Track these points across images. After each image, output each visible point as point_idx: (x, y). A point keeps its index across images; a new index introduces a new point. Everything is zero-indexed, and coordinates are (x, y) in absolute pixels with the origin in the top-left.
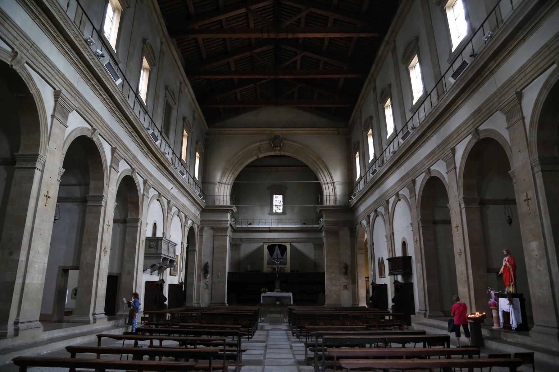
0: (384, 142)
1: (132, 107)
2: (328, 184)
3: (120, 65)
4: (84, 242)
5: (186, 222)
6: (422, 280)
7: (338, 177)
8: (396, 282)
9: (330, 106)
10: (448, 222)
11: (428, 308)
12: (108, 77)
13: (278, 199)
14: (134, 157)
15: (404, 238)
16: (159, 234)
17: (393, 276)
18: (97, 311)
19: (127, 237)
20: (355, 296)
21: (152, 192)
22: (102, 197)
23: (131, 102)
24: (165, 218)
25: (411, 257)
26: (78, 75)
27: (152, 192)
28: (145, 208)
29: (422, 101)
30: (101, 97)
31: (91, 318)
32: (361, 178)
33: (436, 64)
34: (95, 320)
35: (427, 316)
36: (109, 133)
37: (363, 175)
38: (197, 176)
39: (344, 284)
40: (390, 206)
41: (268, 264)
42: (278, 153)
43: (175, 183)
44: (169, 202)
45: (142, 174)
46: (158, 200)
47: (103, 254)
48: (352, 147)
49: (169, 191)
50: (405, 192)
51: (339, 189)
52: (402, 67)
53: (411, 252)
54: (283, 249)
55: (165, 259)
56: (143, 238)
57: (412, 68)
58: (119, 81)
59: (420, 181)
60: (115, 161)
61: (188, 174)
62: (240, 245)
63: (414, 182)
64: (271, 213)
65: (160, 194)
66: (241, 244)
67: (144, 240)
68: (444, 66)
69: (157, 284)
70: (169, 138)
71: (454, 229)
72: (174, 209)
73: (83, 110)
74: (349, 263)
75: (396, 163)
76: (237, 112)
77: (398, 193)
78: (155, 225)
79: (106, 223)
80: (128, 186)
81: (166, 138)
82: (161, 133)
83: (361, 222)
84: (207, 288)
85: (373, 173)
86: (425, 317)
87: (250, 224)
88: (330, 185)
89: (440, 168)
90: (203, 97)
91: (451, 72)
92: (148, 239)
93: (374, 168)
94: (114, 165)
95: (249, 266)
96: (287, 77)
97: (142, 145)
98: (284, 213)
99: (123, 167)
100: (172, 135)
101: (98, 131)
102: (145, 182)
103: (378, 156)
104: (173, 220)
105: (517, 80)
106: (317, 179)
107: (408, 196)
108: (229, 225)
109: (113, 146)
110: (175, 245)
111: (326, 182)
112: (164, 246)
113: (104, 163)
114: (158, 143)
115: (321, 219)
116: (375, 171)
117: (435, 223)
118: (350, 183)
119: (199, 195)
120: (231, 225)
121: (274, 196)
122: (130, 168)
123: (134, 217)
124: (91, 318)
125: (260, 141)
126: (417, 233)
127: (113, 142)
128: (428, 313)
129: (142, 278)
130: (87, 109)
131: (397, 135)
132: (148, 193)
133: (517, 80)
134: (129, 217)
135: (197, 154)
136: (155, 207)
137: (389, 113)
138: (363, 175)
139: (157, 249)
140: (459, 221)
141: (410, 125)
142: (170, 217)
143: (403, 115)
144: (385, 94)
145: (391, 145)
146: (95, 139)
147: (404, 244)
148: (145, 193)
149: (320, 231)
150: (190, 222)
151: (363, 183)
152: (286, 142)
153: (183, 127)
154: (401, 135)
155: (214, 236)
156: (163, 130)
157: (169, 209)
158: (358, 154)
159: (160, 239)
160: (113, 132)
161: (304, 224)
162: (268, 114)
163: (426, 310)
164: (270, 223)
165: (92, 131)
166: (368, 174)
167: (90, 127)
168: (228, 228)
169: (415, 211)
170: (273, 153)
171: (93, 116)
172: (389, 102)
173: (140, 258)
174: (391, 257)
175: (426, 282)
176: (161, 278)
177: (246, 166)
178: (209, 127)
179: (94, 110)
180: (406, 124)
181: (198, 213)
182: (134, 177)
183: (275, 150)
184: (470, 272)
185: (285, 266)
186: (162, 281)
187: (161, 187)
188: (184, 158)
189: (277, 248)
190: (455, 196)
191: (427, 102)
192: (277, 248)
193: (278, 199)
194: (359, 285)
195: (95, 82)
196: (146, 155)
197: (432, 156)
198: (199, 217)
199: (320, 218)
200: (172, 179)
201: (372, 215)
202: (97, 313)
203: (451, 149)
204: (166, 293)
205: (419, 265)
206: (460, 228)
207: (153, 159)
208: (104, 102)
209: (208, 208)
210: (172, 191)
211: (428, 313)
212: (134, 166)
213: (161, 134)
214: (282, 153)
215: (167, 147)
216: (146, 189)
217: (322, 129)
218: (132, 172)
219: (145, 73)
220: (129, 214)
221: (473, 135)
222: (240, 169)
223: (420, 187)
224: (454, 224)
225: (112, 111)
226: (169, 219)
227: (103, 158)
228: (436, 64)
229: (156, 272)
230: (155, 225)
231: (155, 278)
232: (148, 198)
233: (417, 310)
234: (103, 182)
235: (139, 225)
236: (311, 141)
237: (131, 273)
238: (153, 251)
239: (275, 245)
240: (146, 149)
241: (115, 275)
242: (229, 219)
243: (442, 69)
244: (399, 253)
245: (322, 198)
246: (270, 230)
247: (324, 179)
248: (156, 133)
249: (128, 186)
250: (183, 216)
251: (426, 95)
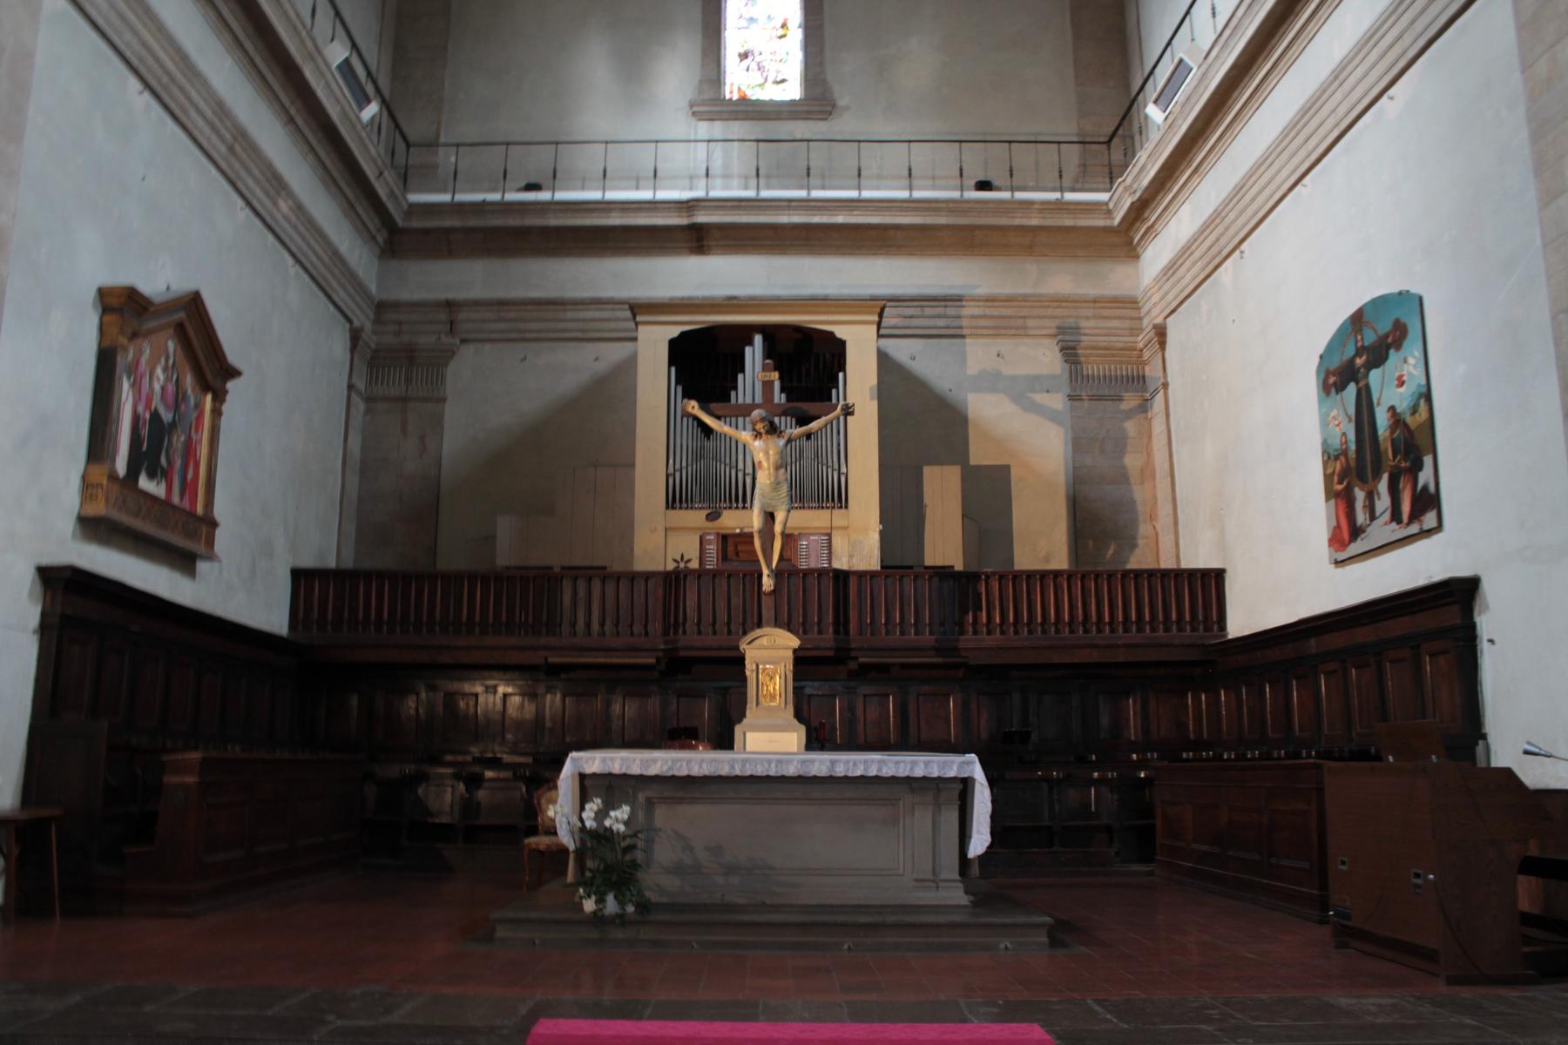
41: (674, 501)
54: (809, 364)
62: (440, 359)
66: (452, 353)
87: (532, 187)
95: (505, 528)
98: (819, 97)
105: (1232, 216)
109: (356, 323)
133: (1232, 216)
155: (1347, 934)
164: (686, 165)
185: (839, 517)
189: (754, 354)
192: (754, 354)
203: (1155, 327)
225: (350, 208)
239: (743, 334)
246: (697, 236)
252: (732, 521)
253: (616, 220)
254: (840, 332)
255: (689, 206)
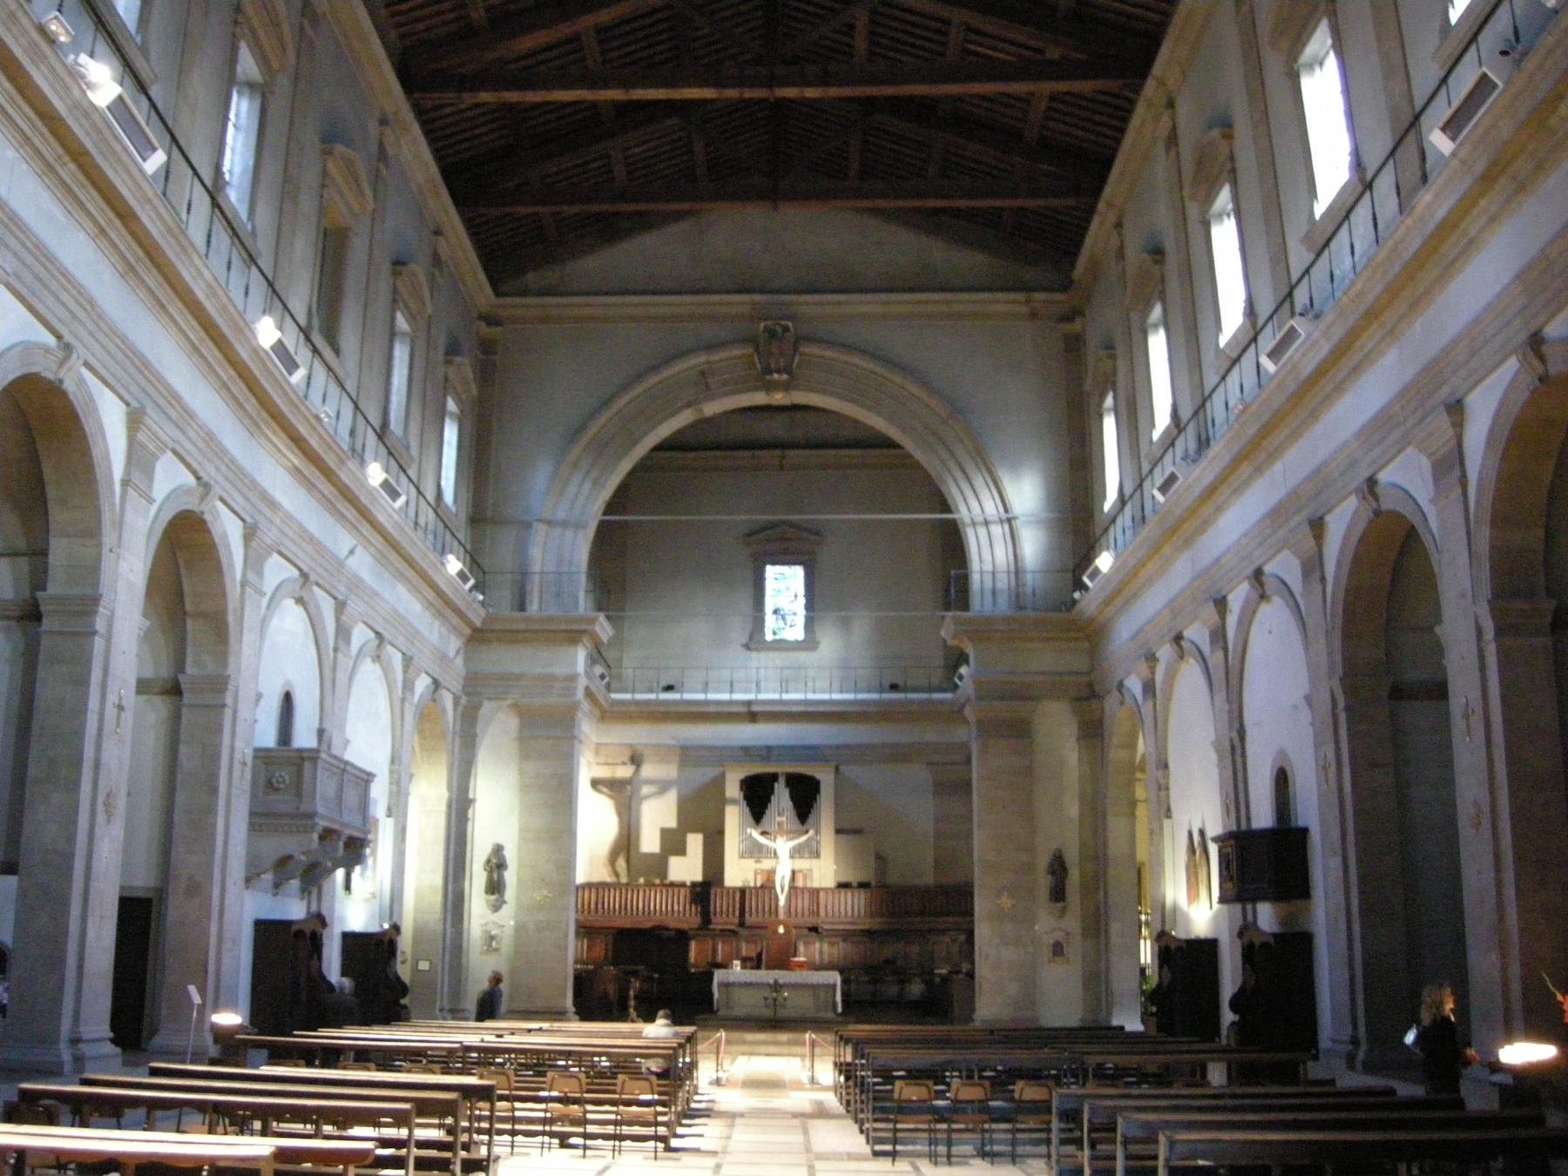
0: (1208, 357)
1: (203, 250)
2: (986, 523)
3: (155, 91)
4: (32, 772)
5: (408, 686)
6: (1343, 926)
7: (1026, 492)
8: (1245, 930)
9: (998, 203)
10: (1439, 691)
11: (1362, 1030)
12: (118, 148)
13: (785, 585)
14: (210, 437)
15: (1282, 754)
16: (304, 738)
17: (1238, 907)
18: (87, 1031)
19: (184, 750)
20: (1097, 983)
21: (277, 571)
22: (95, 600)
23: (197, 228)
24: (327, 672)
25: (1304, 832)
26: (11, 153)
27: (277, 571)
28: (249, 638)
29: (1343, 212)
30: (89, 225)
31: (66, 1056)
32: (1122, 500)
33: (1398, 69)
34: (79, 1060)
35: (1359, 1067)
36: (119, 356)
37: (1128, 491)
38: (449, 497)
39: (1049, 940)
40: (1232, 621)
42: (779, 398)
43: (365, 528)
44: (340, 606)
45: (239, 502)
46: (300, 601)
47: (101, 817)
48: (1077, 387)
49: (340, 564)
50: (1285, 566)
51: (1033, 545)
52: (1273, 65)
53: (1310, 811)
55: (327, 834)
56: (244, 751)
57: (1310, 67)
58: (156, 161)
59: (1343, 520)
60: (140, 460)
61: (413, 490)
63: (1317, 527)
64: (755, 639)
65: (304, 575)
67: (249, 760)
68: (1425, 75)
69: (299, 934)
70: (337, 351)
71: (1458, 724)
72: (360, 635)
73: (29, 278)
74: (1072, 856)
75: (1256, 451)
76: (610, 230)
77: (1372, 482)
78: (288, 699)
79: (112, 699)
80: (185, 544)
81: (327, 352)
82: (306, 332)
83: (1120, 686)
84: (673, 1077)
85: (1164, 489)
86: (1351, 1066)
87: (669, 688)
88: (997, 530)
89: (1408, 476)
90: (467, 177)
91: (1442, 111)
92: (262, 755)
93: (1167, 467)
94: (136, 476)
96: (811, 93)
97: (239, 388)
98: (810, 643)
99: (169, 478)
100: (349, 337)
101: (82, 350)
102: (250, 534)
103: (1185, 414)
104: (359, 677)
106: (945, 506)
107: (1294, 579)
108: (580, 694)
109: (135, 404)
110: (366, 779)
111: (980, 519)
112: (325, 786)
113: (100, 473)
114: (298, 377)
115: (963, 670)
116: (1172, 478)
117: (1398, 693)
118: (1077, 523)
119: (461, 575)
120: (589, 693)
121: (769, 568)
122: (192, 480)
123: (211, 668)
124: (66, 1056)
125: (709, 347)
126: (1329, 734)
127: (133, 388)
128: (1361, 1056)
129: (242, 907)
130: (43, 273)
131: (1255, 339)
132: (260, 574)
134: (190, 670)
135: (451, 405)
136: (289, 622)
137: (1225, 238)
138: (1128, 491)
139: (299, 795)
140: (1475, 695)
141: (1301, 297)
142: (345, 663)
143: (1280, 256)
144: (1211, 170)
145: (1233, 379)
146: (69, 385)
147: (1282, 779)
148: (251, 576)
149: (955, 714)
150: (422, 684)
151: (1128, 522)
152: (815, 350)
153: (394, 301)
154: (1268, 341)
156: (316, 322)
157: (343, 632)
158: (1109, 401)
159: (311, 756)
160: (135, 352)
161: (894, 687)
162: (738, 232)
163: (1355, 1042)
165: (60, 354)
166: (1147, 485)
167: (51, 340)
168: (575, 707)
169: (1320, 645)
170: (760, 398)
171: (65, 297)
172: (1224, 198)
173: (233, 830)
174: (1234, 828)
175: (1357, 928)
176: (314, 908)
177: (658, 448)
178: (498, 294)
179: (65, 274)
180: (1290, 295)
181: (454, 645)
182: (207, 517)
183: (769, 387)
184: (1510, 891)
186: (320, 920)
187: (310, 549)
188: (395, 424)
190: (1463, 596)
191: (1362, 214)
193: (785, 585)
194: (1114, 939)
195: (69, 171)
196: (254, 427)
197: (1384, 430)
198: (459, 661)
199: (956, 667)
200: (351, 514)
201: (1238, 597)
202: (85, 1036)
204: (332, 965)
205: (1335, 862)
206: (1477, 720)
207: (281, 441)
208: (104, 243)
209: (497, 627)
210: (352, 562)
211: (1361, 1056)
212: (210, 472)
213: (308, 339)
214: (799, 397)
215: (334, 389)
216: (254, 562)
217: (965, 296)
218: (203, 499)
219: (245, 104)
220: (189, 659)
221: (1524, 361)
222: (626, 466)
223: (1341, 553)
224: (1456, 704)
225: (129, 271)
226: (342, 677)
227: (96, 452)
228: (1398, 69)
229: (295, 884)
230: (288, 699)
231: (294, 909)
232: (262, 594)
233: (1324, 1042)
234: (99, 545)
235: (229, 701)
236: (883, 312)
237: (197, 889)
238: (282, 802)
239: (774, 777)
240: (251, 404)
241: (140, 894)
242: (581, 667)
243: (1415, 92)
244: (1263, 816)
245: (964, 580)
247: (975, 506)
248: (293, 341)
249: (185, 544)
250: (397, 660)
251: (1363, 182)
252: (767, 864)
253: (712, 709)
254: (818, 776)
255: (749, 703)
